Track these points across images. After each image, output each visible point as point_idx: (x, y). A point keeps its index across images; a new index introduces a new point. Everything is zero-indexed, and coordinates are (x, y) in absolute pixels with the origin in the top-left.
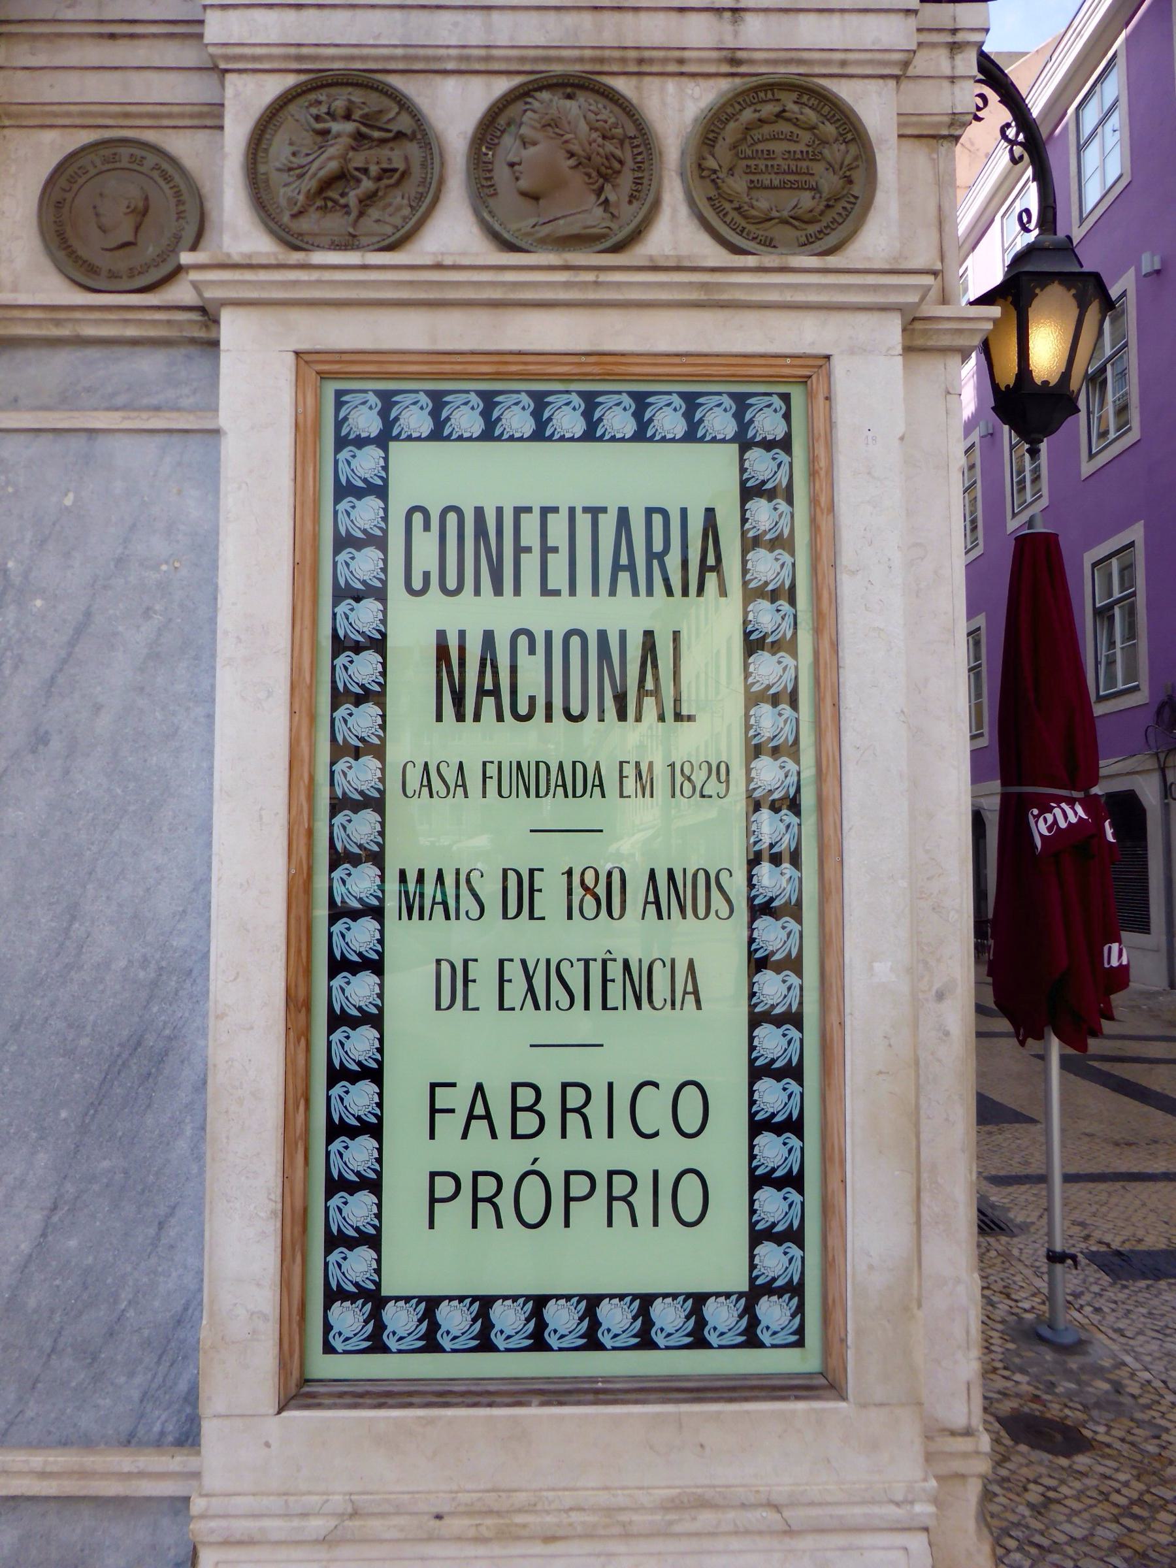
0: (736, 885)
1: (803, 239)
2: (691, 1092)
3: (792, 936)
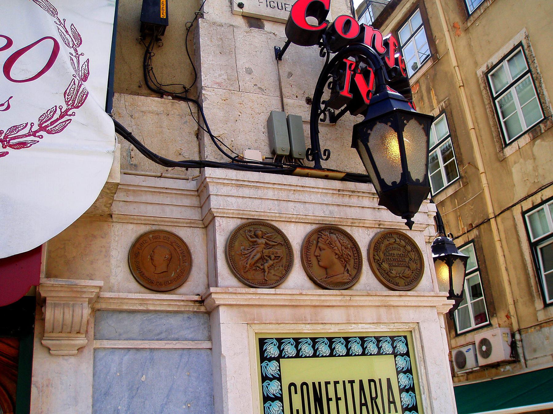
1: (407, 284)
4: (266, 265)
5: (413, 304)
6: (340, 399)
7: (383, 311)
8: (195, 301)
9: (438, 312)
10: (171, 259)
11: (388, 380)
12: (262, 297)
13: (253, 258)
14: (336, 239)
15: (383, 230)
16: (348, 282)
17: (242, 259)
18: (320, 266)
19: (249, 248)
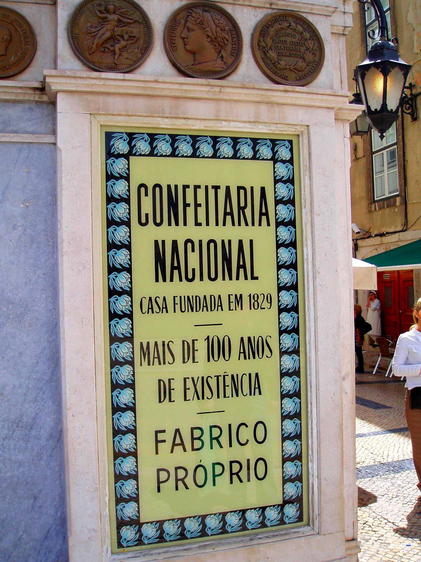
1: (298, 78)
2: (260, 426)
3: (296, 361)
4: (117, 47)
5: (303, 103)
6: (200, 205)
7: (263, 108)
8: (35, 89)
9: (337, 118)
10: (11, 40)
11: (263, 189)
12: (108, 83)
13: (101, 37)
14: (210, 18)
15: (275, 11)
16: (221, 71)
17: (88, 38)
18: (187, 50)
19: (97, 26)
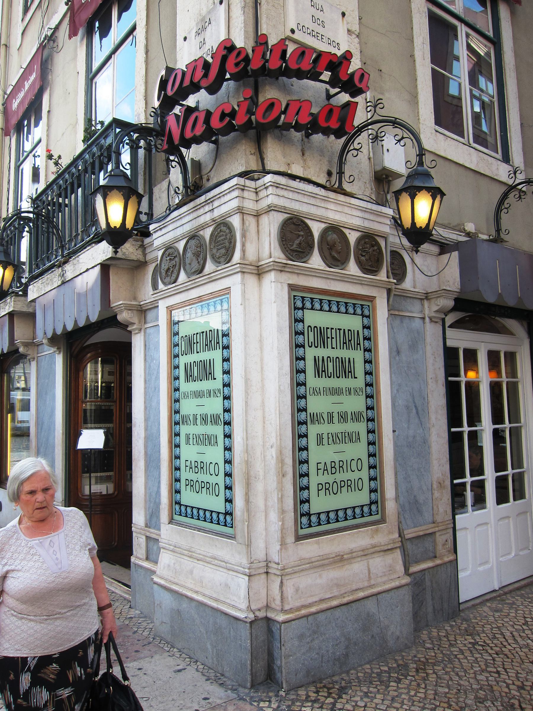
0: (364, 415)
6: (333, 338)
11: (358, 331)
